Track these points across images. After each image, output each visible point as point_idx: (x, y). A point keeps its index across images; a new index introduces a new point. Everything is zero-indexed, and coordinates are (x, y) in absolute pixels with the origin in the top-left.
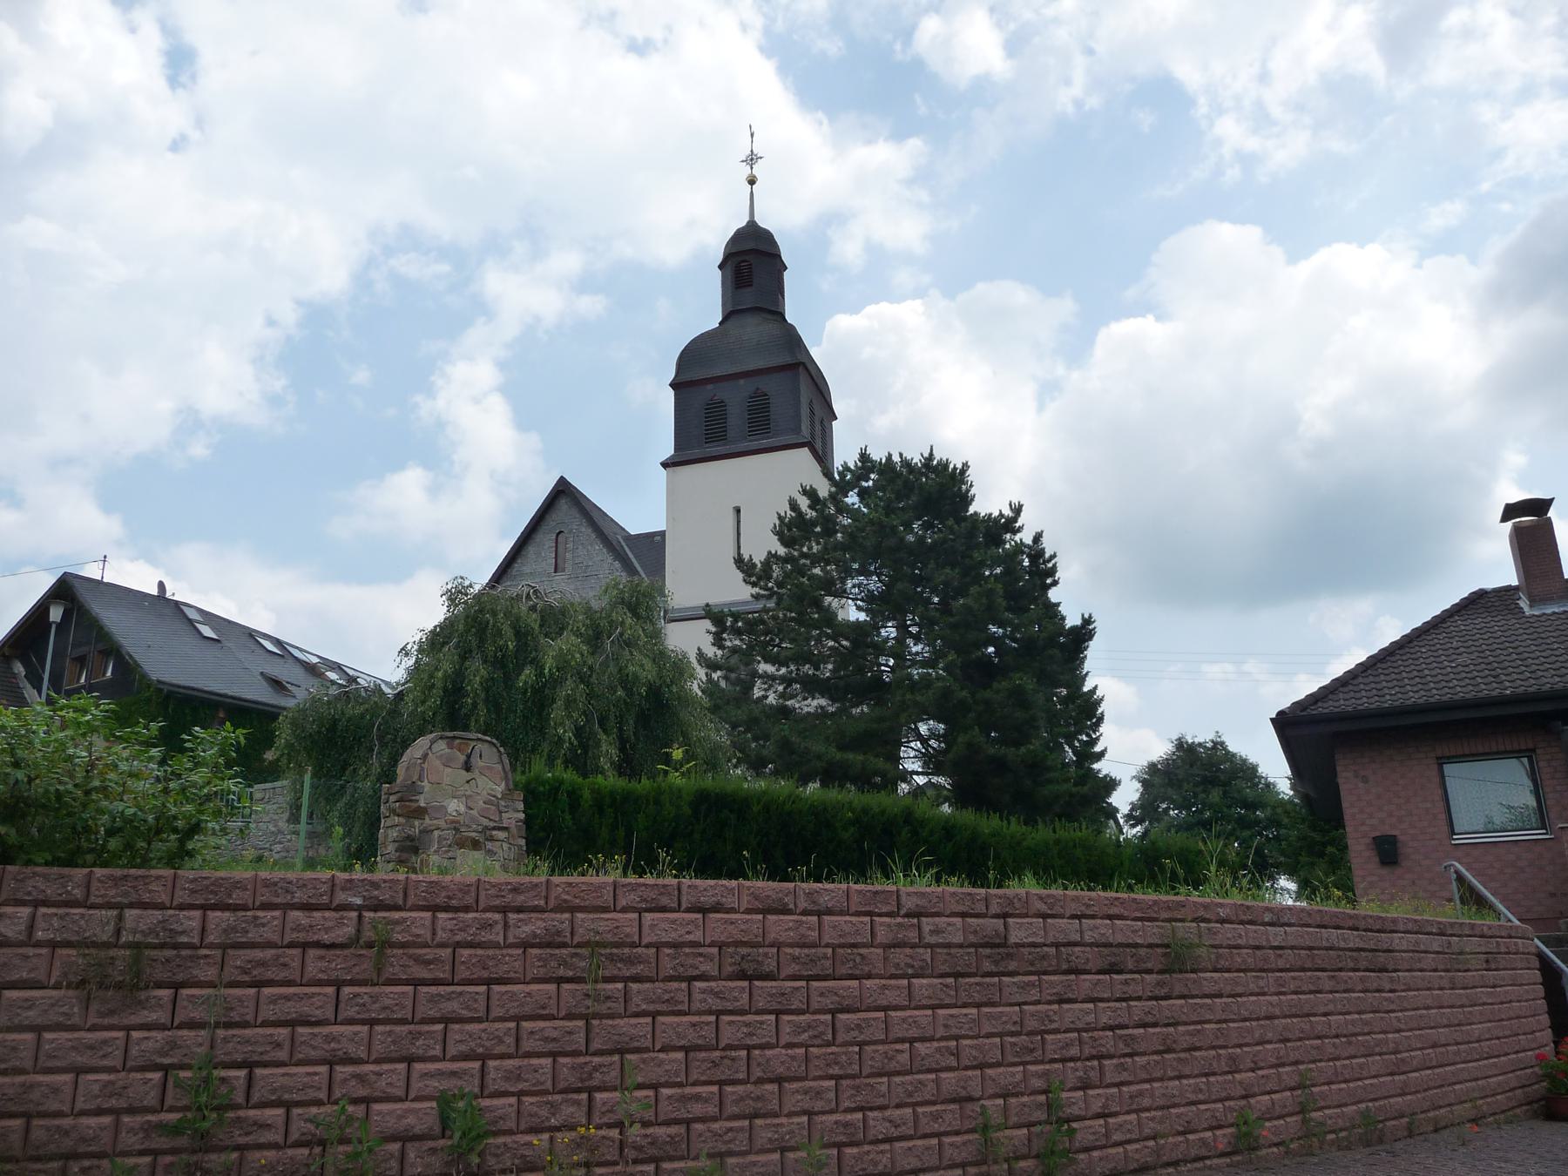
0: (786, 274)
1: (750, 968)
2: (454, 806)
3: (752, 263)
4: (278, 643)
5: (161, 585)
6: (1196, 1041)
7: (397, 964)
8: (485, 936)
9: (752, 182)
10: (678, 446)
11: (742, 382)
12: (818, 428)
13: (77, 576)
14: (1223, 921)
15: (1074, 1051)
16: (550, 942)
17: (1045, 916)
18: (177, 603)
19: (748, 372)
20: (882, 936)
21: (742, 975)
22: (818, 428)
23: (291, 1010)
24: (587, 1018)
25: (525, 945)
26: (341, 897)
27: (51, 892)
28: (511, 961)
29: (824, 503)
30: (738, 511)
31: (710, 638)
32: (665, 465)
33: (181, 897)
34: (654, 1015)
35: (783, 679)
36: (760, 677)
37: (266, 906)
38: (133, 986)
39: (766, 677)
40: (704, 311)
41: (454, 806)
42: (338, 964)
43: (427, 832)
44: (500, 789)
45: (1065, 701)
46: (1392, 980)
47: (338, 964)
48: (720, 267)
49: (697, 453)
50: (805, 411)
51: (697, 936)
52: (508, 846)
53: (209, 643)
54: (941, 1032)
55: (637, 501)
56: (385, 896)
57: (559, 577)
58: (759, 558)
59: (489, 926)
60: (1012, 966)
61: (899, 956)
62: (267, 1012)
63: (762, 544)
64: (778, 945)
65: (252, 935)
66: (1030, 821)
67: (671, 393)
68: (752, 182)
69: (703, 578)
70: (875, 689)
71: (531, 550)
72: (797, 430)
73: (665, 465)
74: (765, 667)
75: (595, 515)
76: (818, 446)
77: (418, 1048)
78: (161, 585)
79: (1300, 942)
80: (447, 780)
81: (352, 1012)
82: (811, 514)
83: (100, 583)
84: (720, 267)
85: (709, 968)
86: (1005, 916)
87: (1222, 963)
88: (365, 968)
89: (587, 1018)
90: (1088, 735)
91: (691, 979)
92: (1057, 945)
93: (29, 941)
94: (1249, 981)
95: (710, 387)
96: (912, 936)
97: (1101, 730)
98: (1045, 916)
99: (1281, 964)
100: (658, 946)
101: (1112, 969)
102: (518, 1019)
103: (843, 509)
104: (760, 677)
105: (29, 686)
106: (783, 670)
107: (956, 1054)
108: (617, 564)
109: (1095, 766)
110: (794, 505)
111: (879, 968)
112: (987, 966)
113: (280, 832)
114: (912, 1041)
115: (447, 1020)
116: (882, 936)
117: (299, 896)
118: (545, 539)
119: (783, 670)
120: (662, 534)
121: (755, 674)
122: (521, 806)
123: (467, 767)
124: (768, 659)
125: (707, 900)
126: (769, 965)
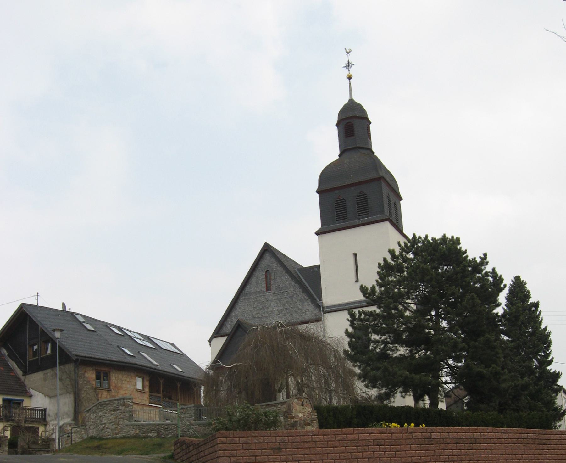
0: (371, 126)
1: (379, 444)
2: (300, 415)
3: (353, 124)
4: (119, 328)
5: (64, 305)
6: (479, 459)
7: (318, 444)
8: (332, 439)
9: (350, 78)
10: (323, 223)
11: (352, 188)
12: (393, 206)
13: (28, 305)
14: (488, 433)
15: (447, 460)
16: (343, 440)
17: (440, 433)
18: (72, 314)
19: (356, 189)
20: (404, 437)
21: (377, 445)
22: (393, 206)
23: (303, 452)
24: (351, 453)
25: (339, 441)
26: (309, 434)
27: (266, 435)
28: (337, 444)
29: (397, 257)
30: (355, 255)
31: (349, 323)
32: (317, 233)
33: (284, 435)
34: (362, 452)
35: (383, 342)
36: (373, 342)
37: (297, 436)
38: (279, 449)
39: (376, 342)
40: (329, 150)
41: (300, 415)
42: (310, 445)
43: (296, 422)
44: (311, 410)
45: (532, 334)
46: (548, 447)
47: (310, 445)
48: (337, 125)
49: (332, 226)
50: (386, 200)
51: (369, 438)
52: (316, 424)
53: (91, 332)
54: (417, 455)
55: (303, 245)
56: (315, 433)
57: (268, 294)
58: (369, 287)
59: (333, 438)
60: (433, 443)
61: (408, 441)
62: (300, 453)
63: (370, 278)
64: (384, 439)
65: (296, 441)
66: (158, 457)
67: (317, 195)
68: (350, 78)
69: (342, 288)
70: (427, 342)
71: (253, 280)
72: (382, 212)
73: (317, 233)
74: (375, 337)
75: (283, 260)
76: (393, 217)
77: (324, 458)
78: (64, 305)
79: (513, 437)
80: (298, 409)
81: (313, 452)
82: (392, 263)
83: (37, 307)
84: (337, 125)
85: (371, 444)
86: (431, 433)
87: (488, 442)
88: (314, 446)
89: (351, 453)
90: (544, 352)
91: (368, 446)
92: (443, 438)
93: (264, 442)
94: (496, 446)
95: (337, 192)
96: (411, 437)
97: (551, 348)
98: (440, 433)
99: (506, 442)
100: (362, 440)
101: (457, 443)
102: (339, 453)
103: (406, 260)
104: (373, 342)
105: (10, 360)
106: (383, 337)
107: (421, 460)
108: (297, 286)
109: (549, 368)
110: (385, 260)
111: (404, 443)
112: (427, 443)
113: (191, 424)
114: (411, 457)
115: (327, 454)
116: (404, 437)
117: (302, 434)
118: (260, 274)
119: (383, 337)
120: (318, 267)
121: (370, 340)
122: (316, 414)
123: (302, 405)
124: (377, 333)
125: (370, 432)
126: (383, 443)
